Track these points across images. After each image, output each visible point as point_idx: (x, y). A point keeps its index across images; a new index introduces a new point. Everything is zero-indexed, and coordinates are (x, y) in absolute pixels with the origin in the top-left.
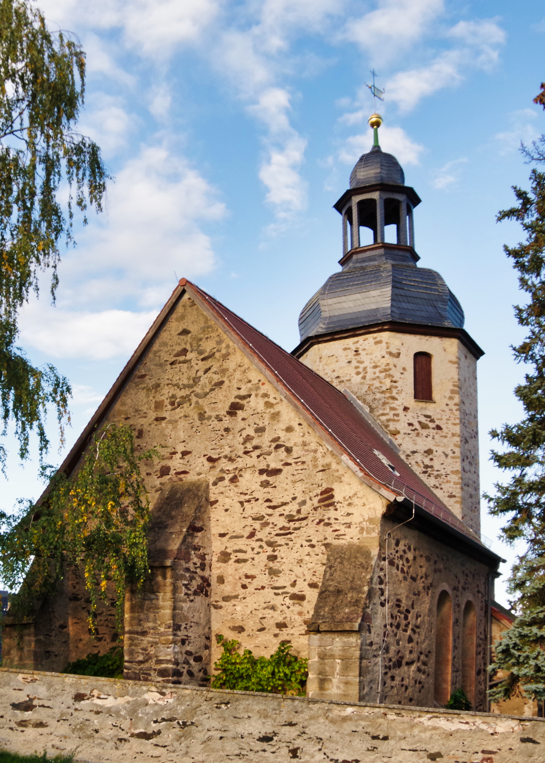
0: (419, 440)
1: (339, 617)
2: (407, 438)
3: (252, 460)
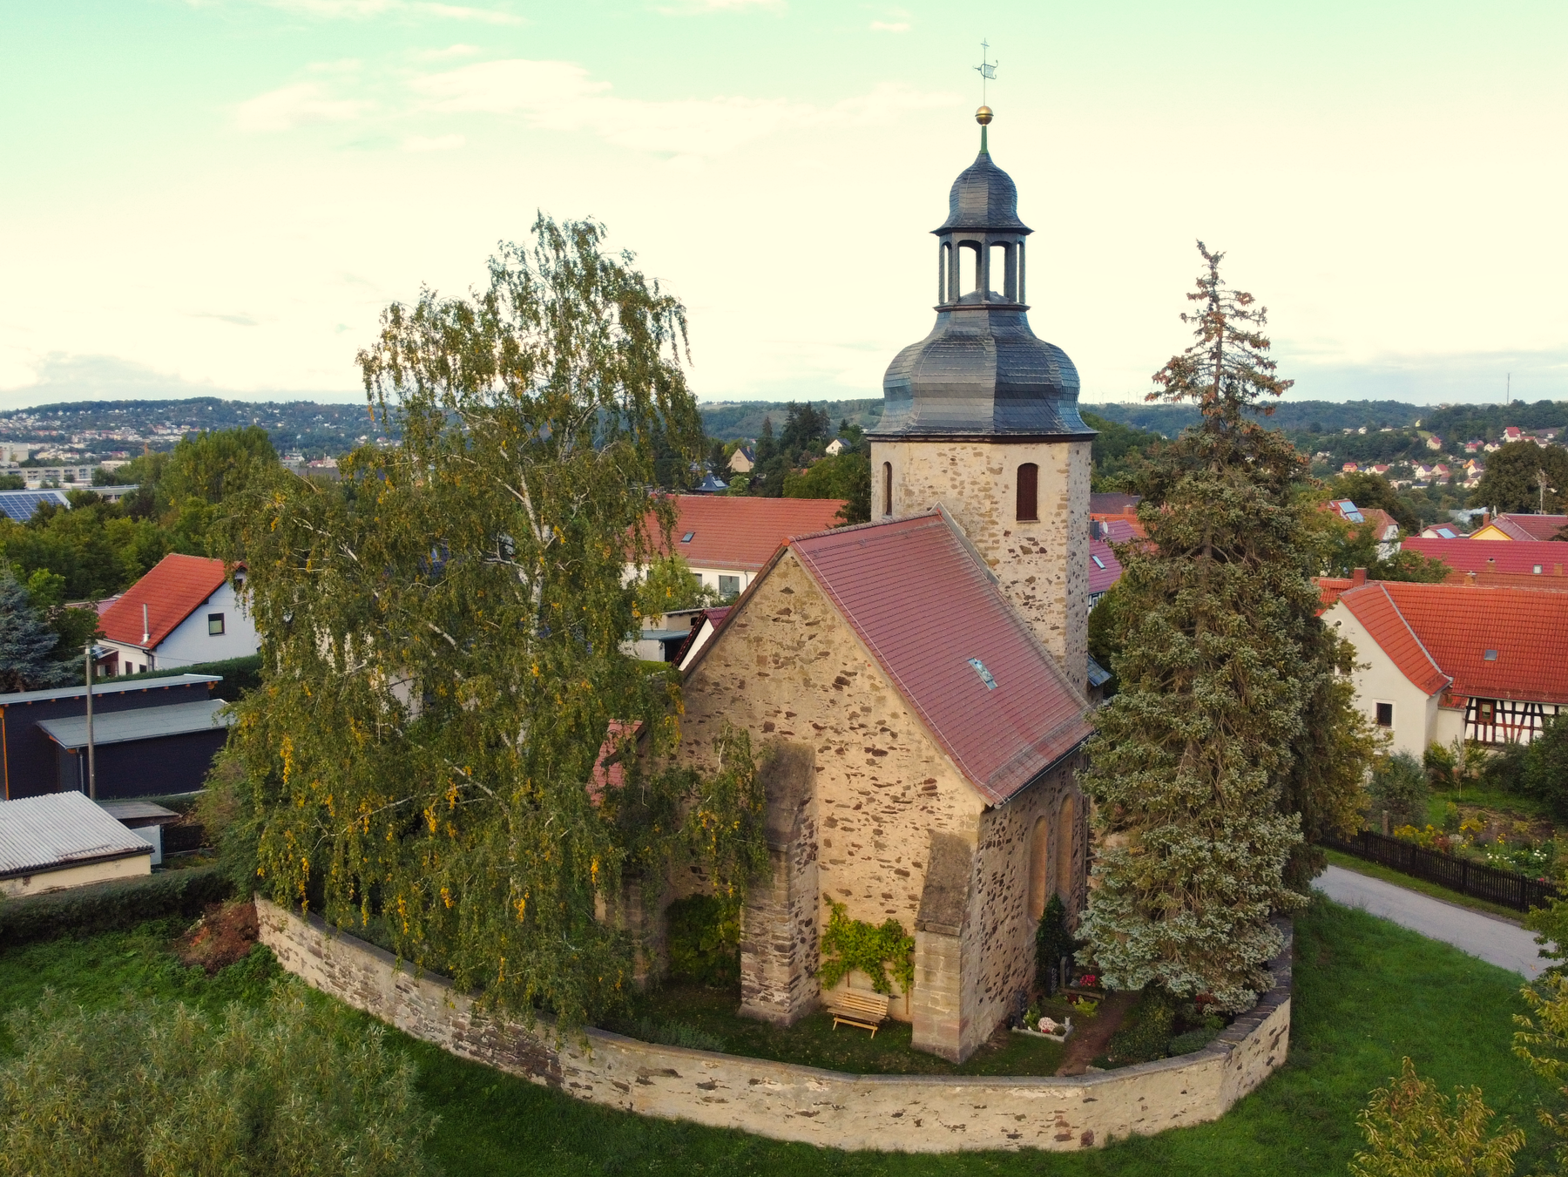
0: (1020, 567)
1: (942, 918)
2: (1008, 567)
3: (857, 737)
